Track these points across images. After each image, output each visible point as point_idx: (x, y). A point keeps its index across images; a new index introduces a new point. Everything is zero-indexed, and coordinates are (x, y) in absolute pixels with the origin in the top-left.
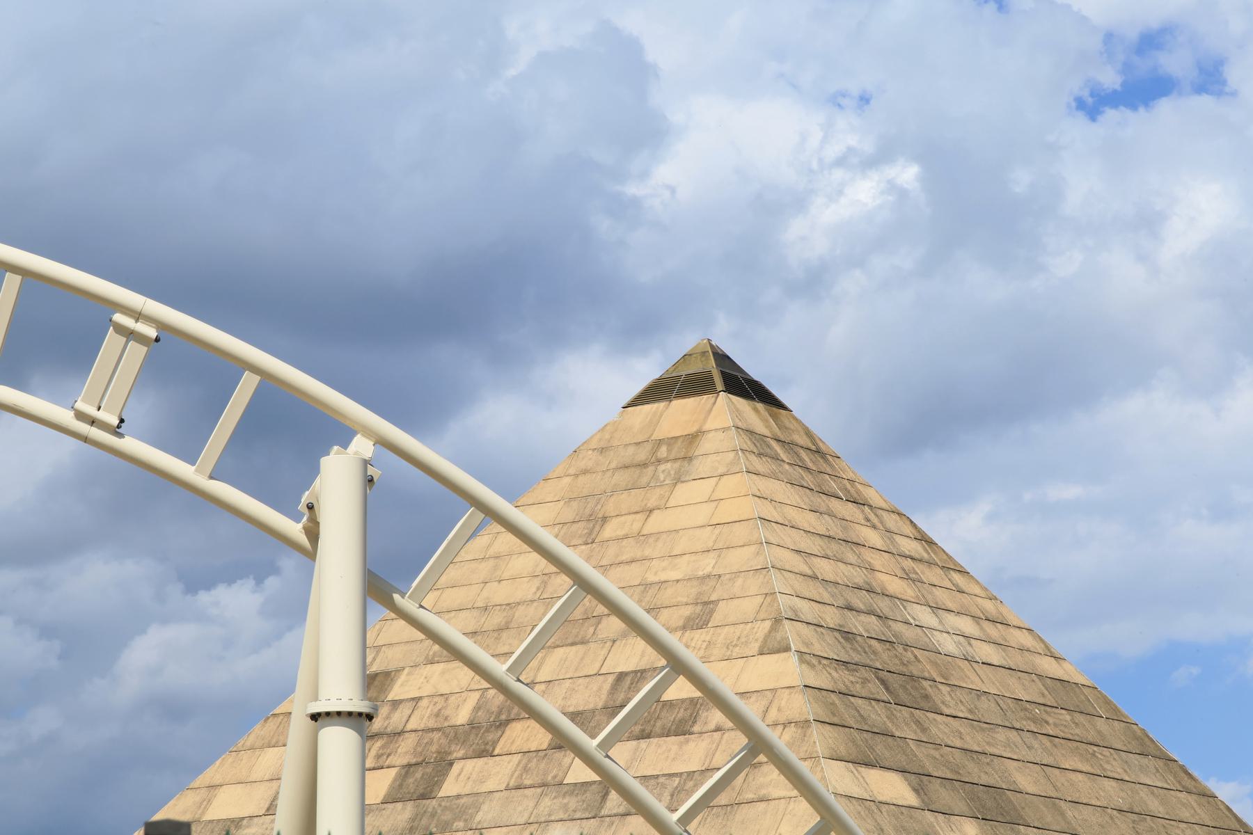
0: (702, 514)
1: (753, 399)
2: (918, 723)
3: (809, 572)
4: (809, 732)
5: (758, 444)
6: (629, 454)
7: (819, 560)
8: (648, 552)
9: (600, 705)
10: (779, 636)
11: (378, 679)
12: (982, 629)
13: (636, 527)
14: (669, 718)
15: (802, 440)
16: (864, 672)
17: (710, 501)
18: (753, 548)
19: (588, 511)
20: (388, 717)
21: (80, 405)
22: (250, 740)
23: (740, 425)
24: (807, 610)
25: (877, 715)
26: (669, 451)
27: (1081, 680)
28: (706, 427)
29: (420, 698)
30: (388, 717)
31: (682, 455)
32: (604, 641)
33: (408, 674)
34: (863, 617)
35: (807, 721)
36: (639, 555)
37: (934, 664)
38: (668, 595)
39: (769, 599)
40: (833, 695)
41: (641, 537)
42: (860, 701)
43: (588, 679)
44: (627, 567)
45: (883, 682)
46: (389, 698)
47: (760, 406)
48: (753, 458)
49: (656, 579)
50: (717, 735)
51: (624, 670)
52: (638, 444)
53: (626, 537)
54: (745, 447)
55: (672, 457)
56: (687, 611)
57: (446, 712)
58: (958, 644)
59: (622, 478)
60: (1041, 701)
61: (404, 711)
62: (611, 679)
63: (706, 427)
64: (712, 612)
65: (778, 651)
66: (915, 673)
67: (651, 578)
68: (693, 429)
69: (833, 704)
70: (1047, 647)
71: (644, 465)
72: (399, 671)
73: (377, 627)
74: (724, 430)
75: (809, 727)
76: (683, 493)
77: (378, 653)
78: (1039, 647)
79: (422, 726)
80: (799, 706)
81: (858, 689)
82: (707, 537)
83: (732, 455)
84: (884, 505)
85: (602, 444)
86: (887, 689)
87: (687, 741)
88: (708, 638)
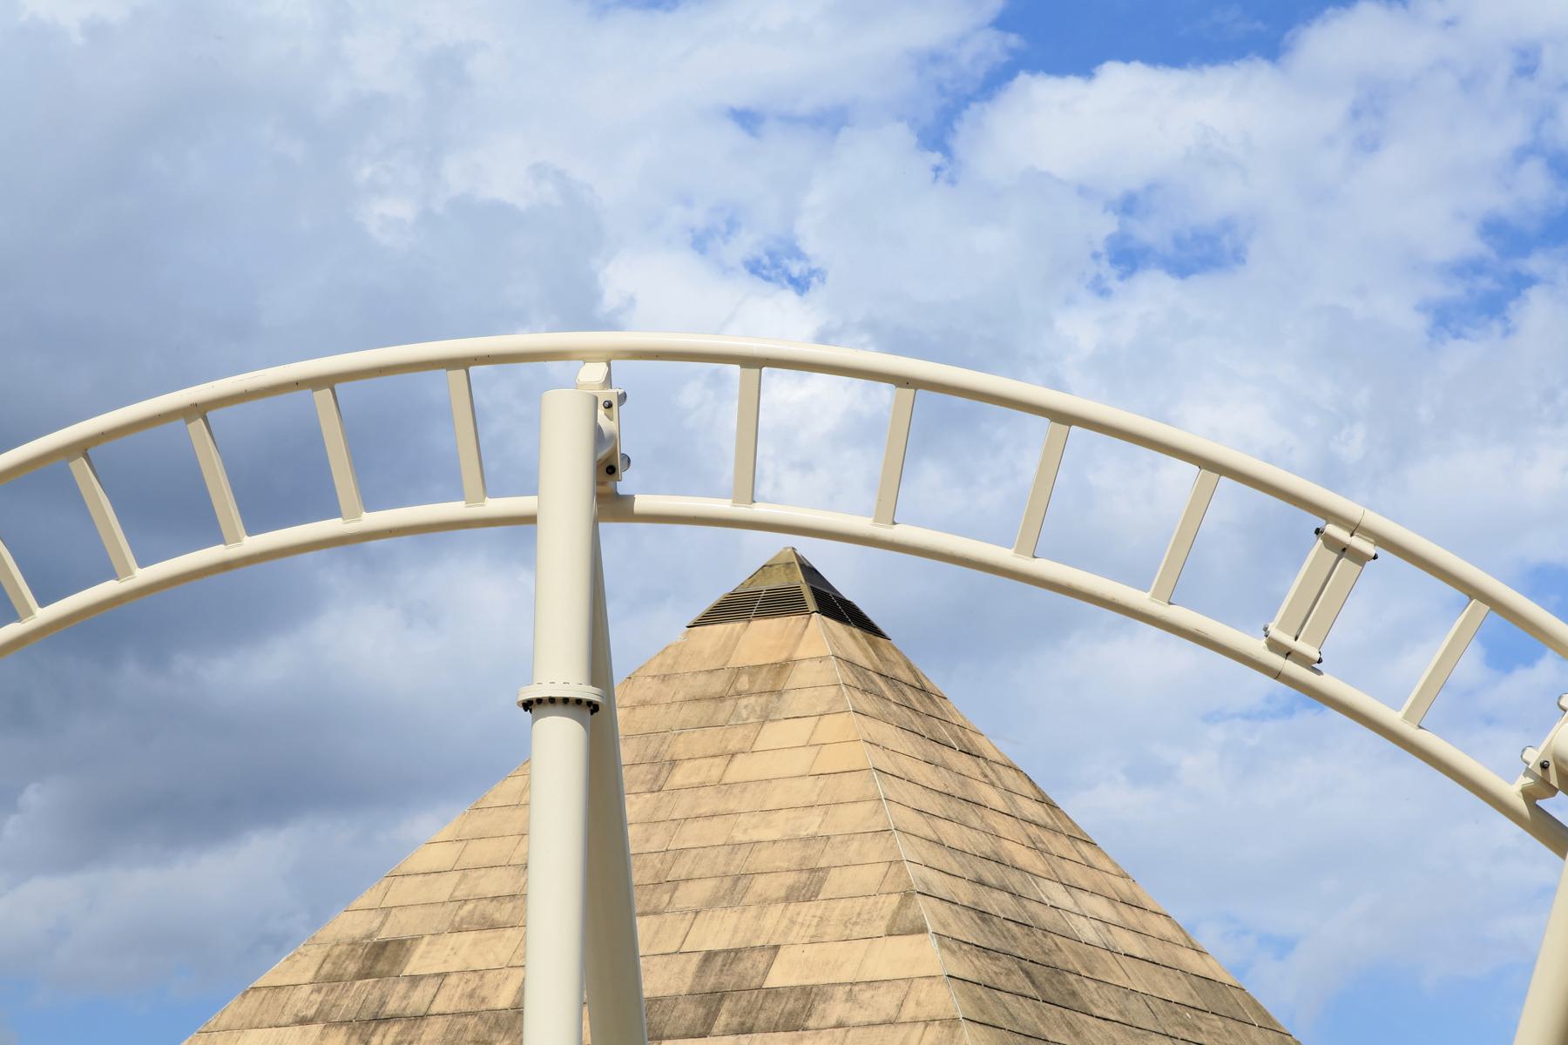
0: (801, 761)
1: (848, 623)
2: (1069, 1025)
3: (934, 837)
4: (958, 1032)
5: (862, 680)
6: (699, 684)
7: (941, 822)
8: (732, 805)
9: (684, 991)
10: (911, 914)
11: (389, 948)
12: (1118, 913)
13: (715, 774)
14: (775, 1010)
15: (905, 675)
16: (1006, 962)
17: (809, 745)
18: (870, 805)
19: (650, 752)
20: (405, 997)
21: (1275, 633)
22: (225, 1019)
23: (839, 653)
24: (940, 884)
25: (1027, 1014)
26: (752, 682)
27: (1228, 980)
28: (797, 655)
29: (445, 975)
30: (405, 997)
31: (769, 688)
32: (684, 912)
33: (429, 944)
34: (996, 894)
35: (955, 1019)
36: (721, 808)
37: (1076, 953)
38: (763, 858)
39: (894, 868)
40: (978, 988)
41: (722, 786)
42: (1007, 997)
43: (666, 958)
44: (707, 822)
45: (1028, 974)
46: (407, 972)
47: (857, 631)
48: (858, 695)
49: (745, 838)
50: (839, 1032)
51: (712, 948)
52: (710, 672)
53: (703, 785)
54: (848, 682)
55: (756, 689)
56: (790, 879)
57: (484, 992)
58: (1097, 930)
59: (693, 712)
60: (1191, 1003)
61: (427, 989)
62: (696, 959)
63: (798, 654)
64: (822, 881)
65: (911, 932)
66: (1059, 964)
67: (739, 837)
68: (781, 657)
69: (980, 998)
70: (1188, 938)
71: (720, 698)
72: (416, 939)
73: (384, 884)
74: (822, 659)
75: (958, 1026)
76: (773, 734)
77: (387, 916)
78: (1181, 940)
79: (452, 1009)
80: (946, 1000)
81: (1002, 981)
82: (807, 790)
83: (833, 690)
84: (998, 758)
85: (664, 671)
86: (1033, 983)
87: (801, 1038)
88: (819, 913)
